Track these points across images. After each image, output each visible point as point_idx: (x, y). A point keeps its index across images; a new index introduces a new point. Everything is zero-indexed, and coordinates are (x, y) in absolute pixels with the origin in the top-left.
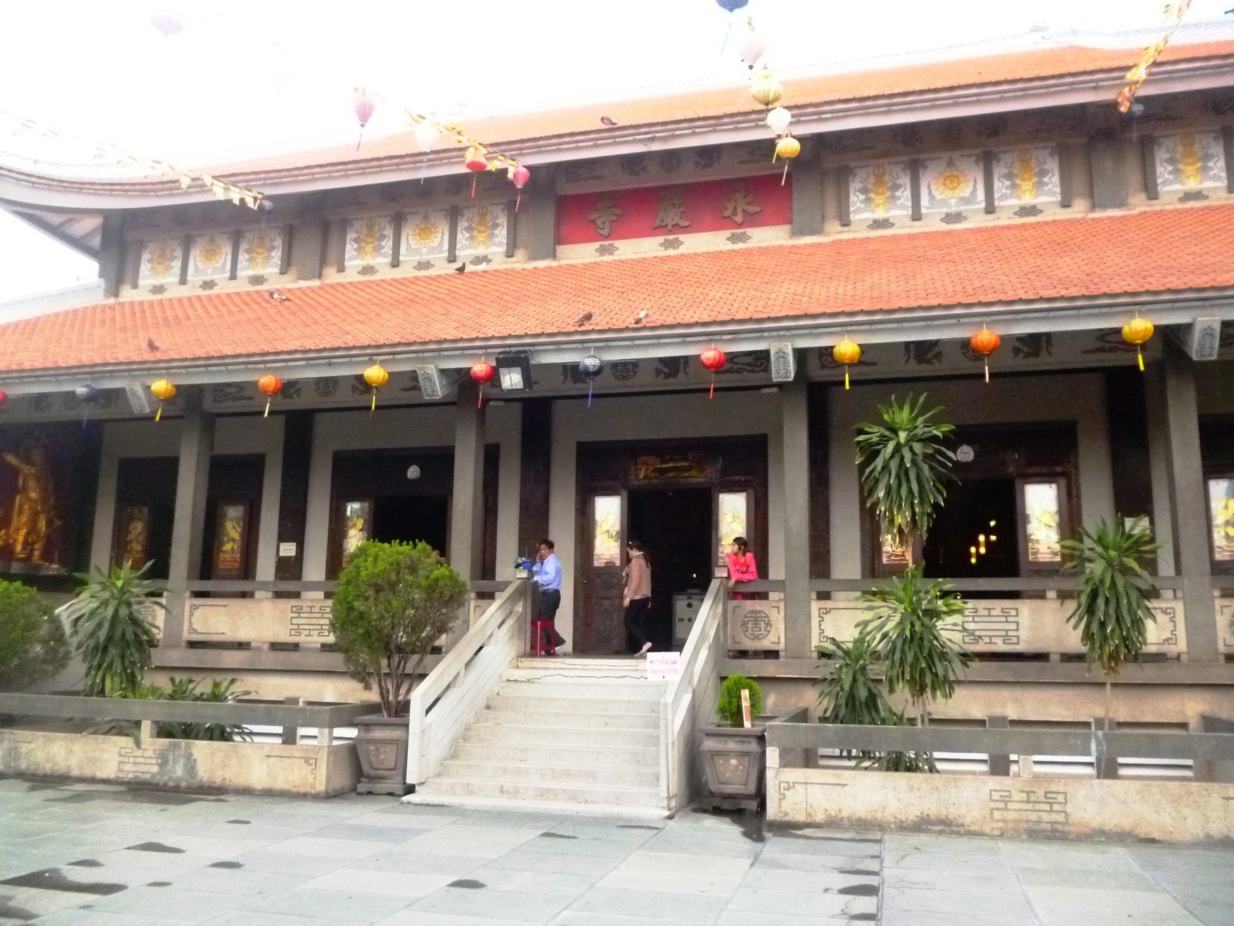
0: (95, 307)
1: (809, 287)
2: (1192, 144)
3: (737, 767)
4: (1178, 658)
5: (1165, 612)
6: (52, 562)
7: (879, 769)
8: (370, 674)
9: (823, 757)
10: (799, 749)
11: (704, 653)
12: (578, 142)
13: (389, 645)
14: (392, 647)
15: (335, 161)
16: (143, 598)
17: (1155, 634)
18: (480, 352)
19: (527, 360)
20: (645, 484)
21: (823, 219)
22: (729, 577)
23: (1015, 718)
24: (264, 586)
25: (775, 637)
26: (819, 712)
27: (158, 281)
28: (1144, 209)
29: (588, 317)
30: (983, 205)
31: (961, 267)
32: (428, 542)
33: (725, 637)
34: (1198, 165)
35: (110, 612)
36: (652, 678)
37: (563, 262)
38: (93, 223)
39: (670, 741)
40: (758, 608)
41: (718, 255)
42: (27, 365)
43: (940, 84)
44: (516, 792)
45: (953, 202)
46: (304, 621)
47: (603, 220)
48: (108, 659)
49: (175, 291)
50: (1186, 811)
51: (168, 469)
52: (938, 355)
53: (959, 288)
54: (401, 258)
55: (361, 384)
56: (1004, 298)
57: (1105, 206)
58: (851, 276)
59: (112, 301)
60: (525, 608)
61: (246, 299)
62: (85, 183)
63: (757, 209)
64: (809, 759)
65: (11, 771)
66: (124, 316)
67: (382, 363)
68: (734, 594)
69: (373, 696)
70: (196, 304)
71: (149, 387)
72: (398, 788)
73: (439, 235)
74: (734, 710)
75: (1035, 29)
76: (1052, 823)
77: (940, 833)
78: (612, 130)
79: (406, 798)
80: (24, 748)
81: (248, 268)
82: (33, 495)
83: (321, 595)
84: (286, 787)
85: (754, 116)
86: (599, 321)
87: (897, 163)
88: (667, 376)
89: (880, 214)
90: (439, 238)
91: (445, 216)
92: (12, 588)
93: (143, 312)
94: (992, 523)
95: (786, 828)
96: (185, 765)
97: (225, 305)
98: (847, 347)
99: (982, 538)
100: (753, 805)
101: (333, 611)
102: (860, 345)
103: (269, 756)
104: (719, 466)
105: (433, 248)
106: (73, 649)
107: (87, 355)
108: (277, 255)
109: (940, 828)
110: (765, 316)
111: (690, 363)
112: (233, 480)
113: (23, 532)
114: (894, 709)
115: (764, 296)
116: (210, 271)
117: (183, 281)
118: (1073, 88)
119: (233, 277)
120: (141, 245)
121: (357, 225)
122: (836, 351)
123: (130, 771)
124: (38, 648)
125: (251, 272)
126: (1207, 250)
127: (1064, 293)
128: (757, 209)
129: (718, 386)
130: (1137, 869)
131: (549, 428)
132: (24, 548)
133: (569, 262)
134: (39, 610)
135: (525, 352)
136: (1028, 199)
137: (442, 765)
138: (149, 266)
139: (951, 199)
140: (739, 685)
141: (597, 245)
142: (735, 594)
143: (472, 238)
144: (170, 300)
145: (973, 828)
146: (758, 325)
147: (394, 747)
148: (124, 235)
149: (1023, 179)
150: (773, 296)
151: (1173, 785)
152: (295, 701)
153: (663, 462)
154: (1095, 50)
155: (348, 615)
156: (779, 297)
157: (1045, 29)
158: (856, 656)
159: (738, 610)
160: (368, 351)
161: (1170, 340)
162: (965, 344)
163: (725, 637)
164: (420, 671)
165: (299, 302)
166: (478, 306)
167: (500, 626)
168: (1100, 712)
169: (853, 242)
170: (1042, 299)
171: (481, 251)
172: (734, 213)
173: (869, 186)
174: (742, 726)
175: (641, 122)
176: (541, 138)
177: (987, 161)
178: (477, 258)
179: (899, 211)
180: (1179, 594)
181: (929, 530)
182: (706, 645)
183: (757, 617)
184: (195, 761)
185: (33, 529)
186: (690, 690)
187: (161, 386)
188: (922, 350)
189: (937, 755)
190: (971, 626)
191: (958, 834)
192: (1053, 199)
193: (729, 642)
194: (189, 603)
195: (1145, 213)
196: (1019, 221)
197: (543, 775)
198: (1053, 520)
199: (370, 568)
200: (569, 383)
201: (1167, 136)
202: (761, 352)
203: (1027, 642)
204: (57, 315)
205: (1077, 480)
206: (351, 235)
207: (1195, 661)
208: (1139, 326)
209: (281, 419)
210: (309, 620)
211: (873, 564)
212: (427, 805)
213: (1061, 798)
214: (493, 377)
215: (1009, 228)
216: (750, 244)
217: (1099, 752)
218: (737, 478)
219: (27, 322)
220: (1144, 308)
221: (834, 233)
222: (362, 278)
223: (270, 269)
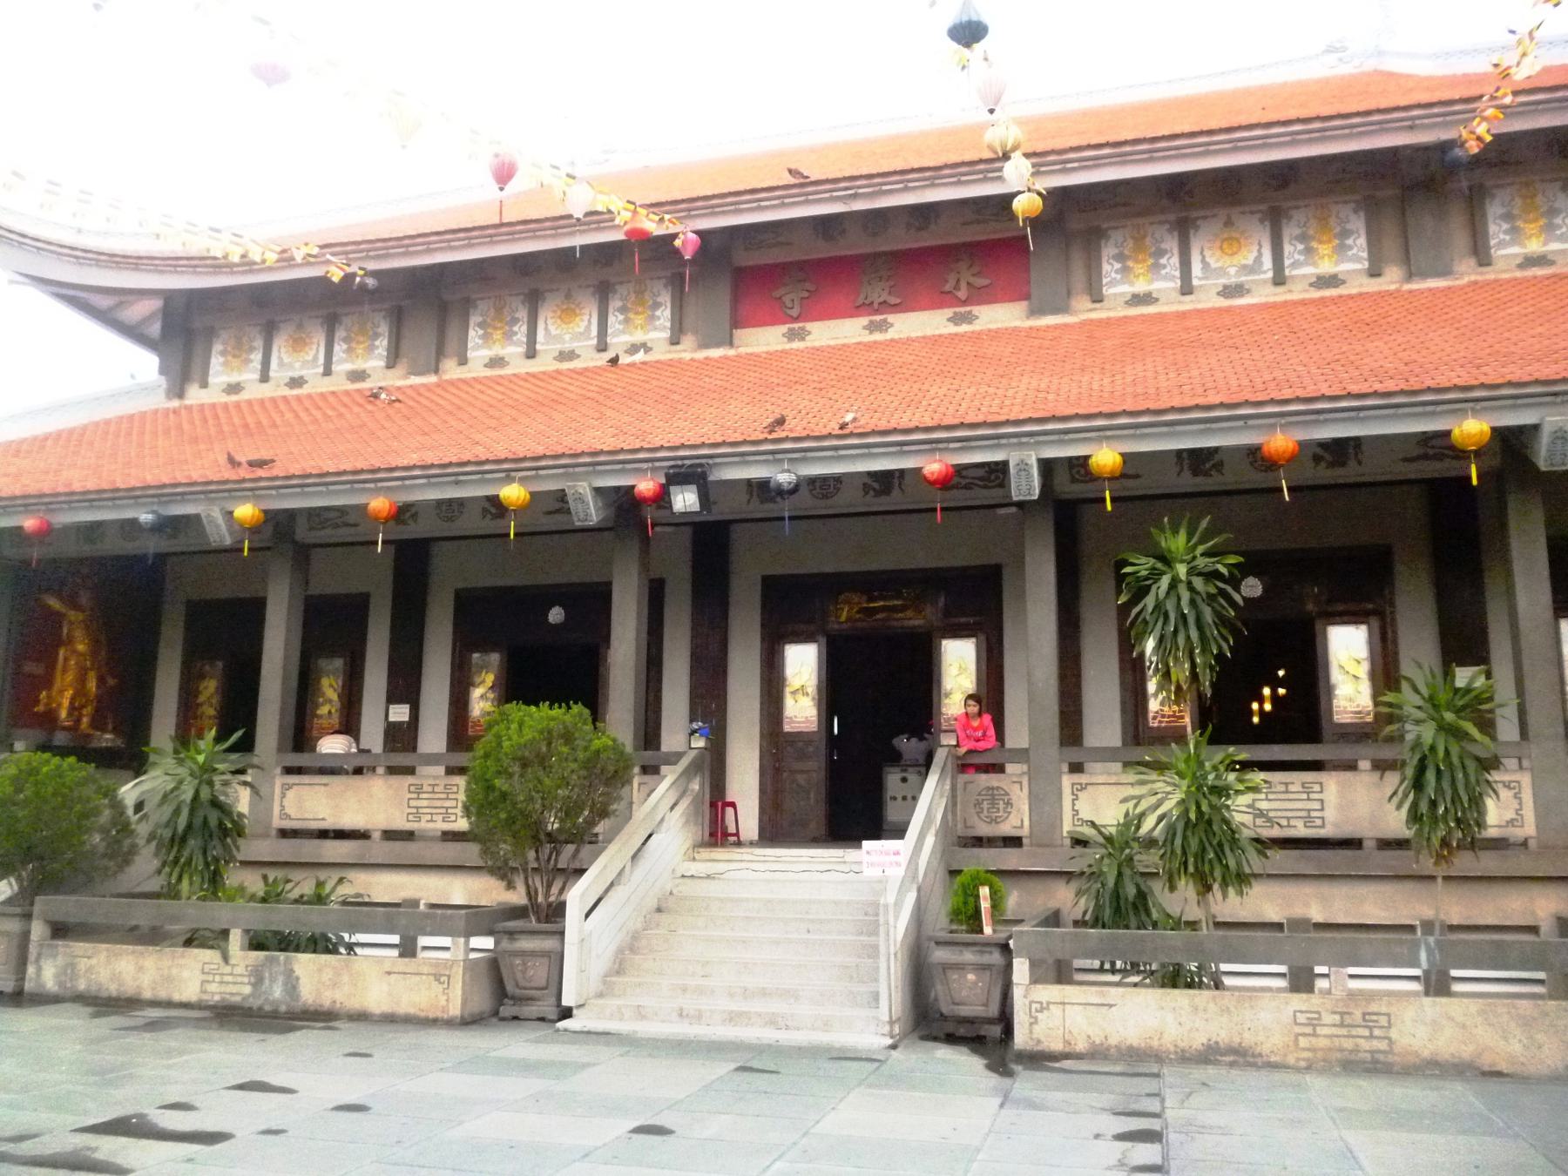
0: (156, 412)
1: (1055, 381)
2: (1144, 237)
3: (975, 983)
4: (1525, 844)
5: (1507, 786)
6: (104, 730)
7: (1152, 986)
8: (514, 869)
9: (1282, 975)
10: (1050, 961)
11: (930, 840)
12: (859, 187)
13: (537, 835)
14: (542, 837)
15: (455, 227)
16: (228, 777)
17: (1497, 814)
18: (645, 466)
19: (703, 476)
20: (849, 630)
21: (1069, 293)
22: (958, 745)
23: (1321, 920)
24: (432, 759)
25: (1018, 820)
26: (1077, 914)
27: (234, 378)
28: (1473, 278)
29: (781, 422)
30: (1270, 274)
31: (1246, 355)
32: (585, 705)
33: (954, 819)
34: (1542, 222)
35: (188, 795)
36: (870, 872)
37: (742, 350)
38: (153, 305)
39: (892, 951)
40: (995, 784)
41: (935, 340)
42: (77, 487)
43: (1214, 124)
44: (699, 1017)
45: (1232, 271)
46: (425, 803)
47: (791, 297)
48: (186, 853)
49: (255, 391)
50: (1540, 1037)
51: (251, 613)
52: (1219, 466)
53: (1245, 382)
54: (538, 347)
55: (495, 506)
56: (1301, 393)
57: (1424, 275)
58: (1107, 366)
59: (176, 403)
60: (702, 785)
61: (346, 399)
62: (140, 258)
63: (985, 282)
64: (1062, 973)
65: (68, 994)
66: (192, 423)
67: (522, 480)
68: (963, 767)
69: (518, 897)
70: (282, 407)
71: (231, 513)
72: (551, 1012)
73: (586, 318)
74: (971, 912)
75: (1330, 50)
76: (1372, 1052)
77: (1232, 1064)
78: (802, 185)
79: (561, 1025)
80: (83, 964)
81: (346, 361)
82: (81, 647)
83: (441, 770)
84: (412, 1011)
85: (982, 167)
86: (795, 426)
87: (1161, 223)
88: (879, 493)
89: (1141, 286)
90: (586, 321)
91: (593, 294)
92: (65, 765)
93: (216, 417)
94: (1281, 673)
95: (1038, 1059)
96: (285, 984)
97: (319, 408)
98: (1106, 457)
99: (1267, 691)
100: (996, 1031)
101: (468, 790)
102: (1123, 455)
103: (389, 973)
104: (942, 602)
105: (1244, 267)
106: (141, 842)
107: (154, 474)
108: (382, 344)
109: (1231, 1058)
110: (1003, 418)
111: (1364, 448)
112: (332, 628)
113: (69, 694)
114: (1169, 911)
115: (1000, 392)
116: (297, 365)
117: (265, 378)
118: (1383, 128)
119: (328, 372)
120: (210, 334)
121: (482, 305)
122: (1093, 461)
123: (216, 992)
124: (97, 838)
125: (349, 366)
126: (1555, 331)
127: (1378, 387)
128: (985, 282)
129: (794, 514)
130: (1479, 1105)
131: (726, 558)
132: (70, 714)
133: (749, 350)
134: (97, 792)
135: (701, 465)
136: (1326, 267)
137: (605, 983)
138: (221, 359)
139: (1230, 268)
140: (977, 881)
141: (784, 328)
142: (964, 766)
143: (627, 321)
144: (249, 403)
145: (1273, 1059)
146: (994, 431)
147: (545, 960)
148: (191, 321)
149: (1321, 242)
150: (1010, 393)
151: (1524, 1004)
152: (414, 903)
153: (871, 600)
154: (1408, 76)
155: (487, 795)
156: (1018, 396)
157: (1344, 49)
158: (1121, 843)
159: (970, 786)
160: (506, 466)
161: (1511, 446)
162: (1253, 452)
163: (954, 819)
164: (577, 865)
165: (411, 403)
166: (639, 407)
167: (672, 808)
168: (1428, 913)
169: (1107, 323)
170: (1350, 396)
171: (638, 336)
172: (957, 287)
173: (1515, 212)
174: (981, 931)
175: (840, 175)
176: (714, 197)
177: (1275, 220)
178: (633, 345)
179: (1164, 284)
180: (1525, 763)
181: (1213, 685)
182: (933, 831)
183: (993, 795)
184: (298, 979)
185: (80, 691)
186: (915, 887)
187: (246, 511)
188: (1198, 460)
189: (1224, 967)
190: (1264, 805)
191: (1253, 1065)
192: (1358, 266)
193: (960, 826)
194: (280, 780)
195: (1476, 283)
196: (1316, 294)
197: (731, 995)
198: (1363, 670)
199: (515, 737)
200: (755, 502)
201: (1502, 186)
202: (996, 463)
203: (1336, 825)
204: (108, 422)
205: (1393, 620)
206: (475, 319)
207: (1545, 848)
208: (1472, 428)
209: (392, 548)
210: (438, 802)
211: (1136, 727)
212: (589, 1033)
213: (1383, 1021)
214: (662, 498)
215: (1303, 303)
216: (977, 326)
217: (1425, 964)
218: (963, 620)
219: (71, 431)
220: (1479, 406)
221: (1083, 311)
222: (489, 372)
223: (374, 361)
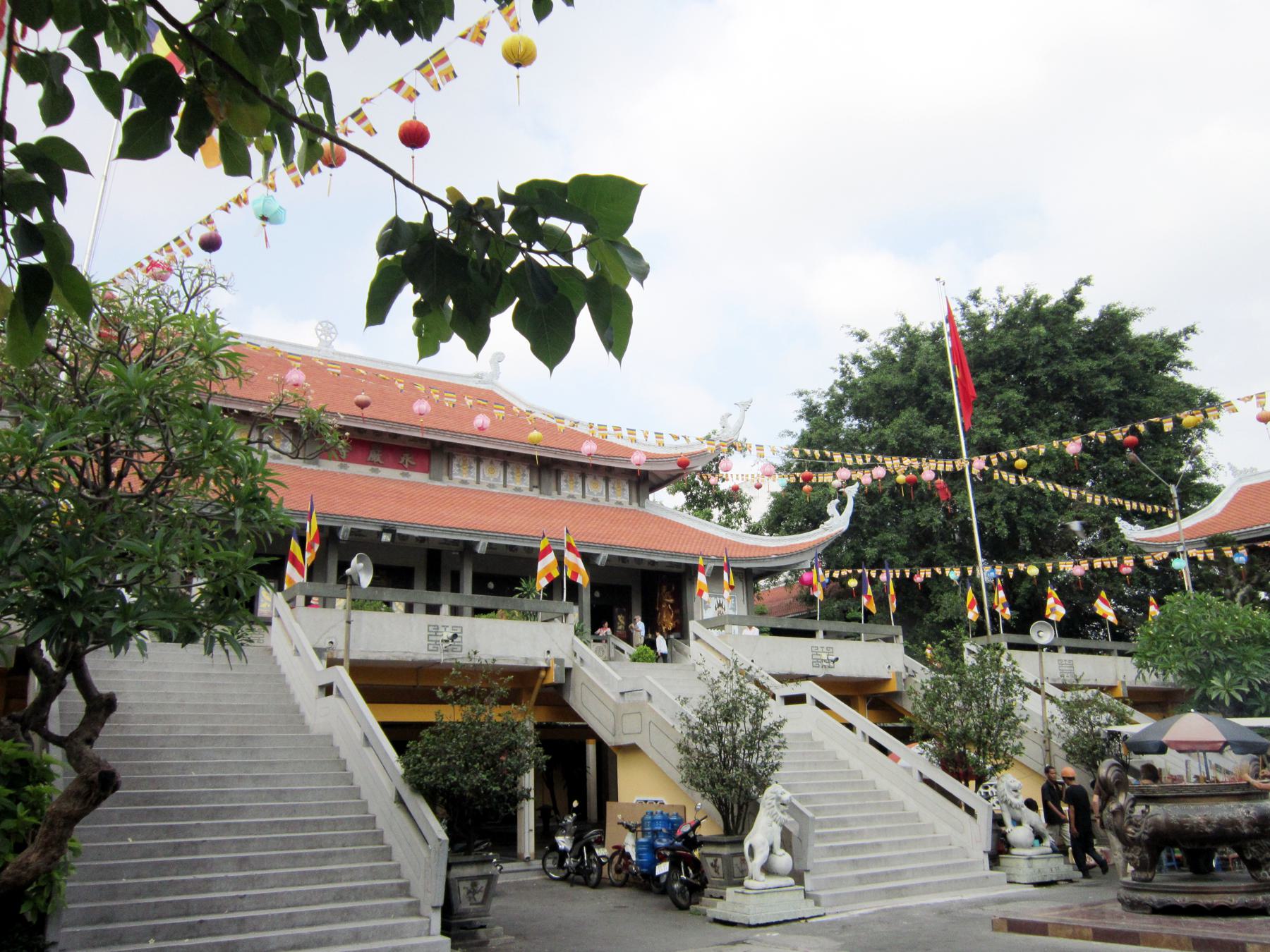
89: (464, 478)
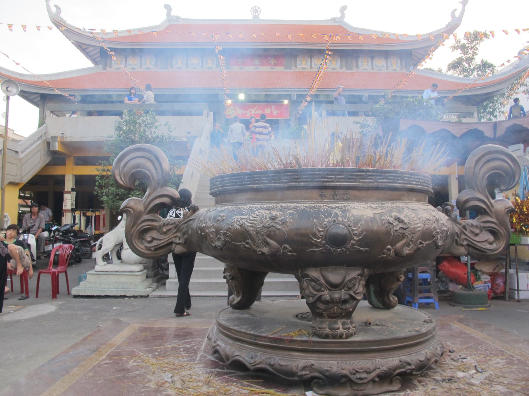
221: (294, 69)
